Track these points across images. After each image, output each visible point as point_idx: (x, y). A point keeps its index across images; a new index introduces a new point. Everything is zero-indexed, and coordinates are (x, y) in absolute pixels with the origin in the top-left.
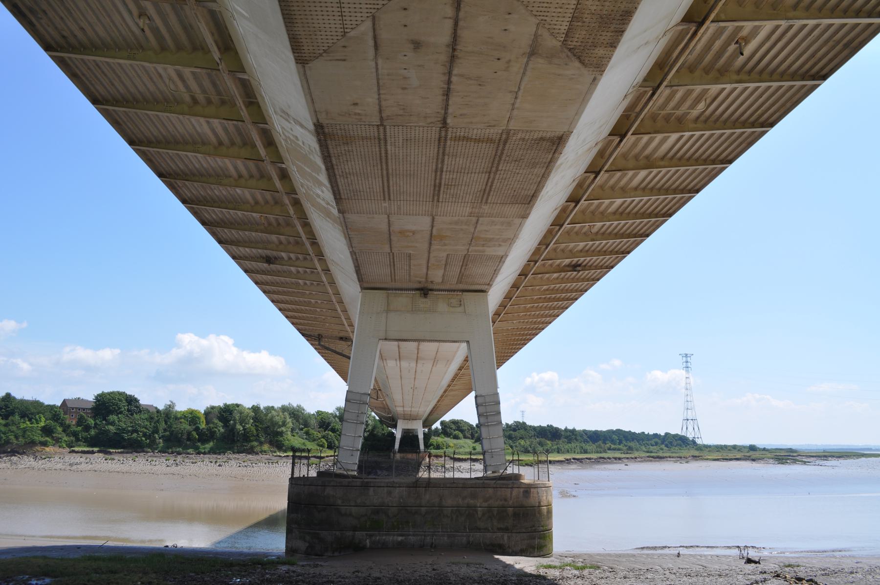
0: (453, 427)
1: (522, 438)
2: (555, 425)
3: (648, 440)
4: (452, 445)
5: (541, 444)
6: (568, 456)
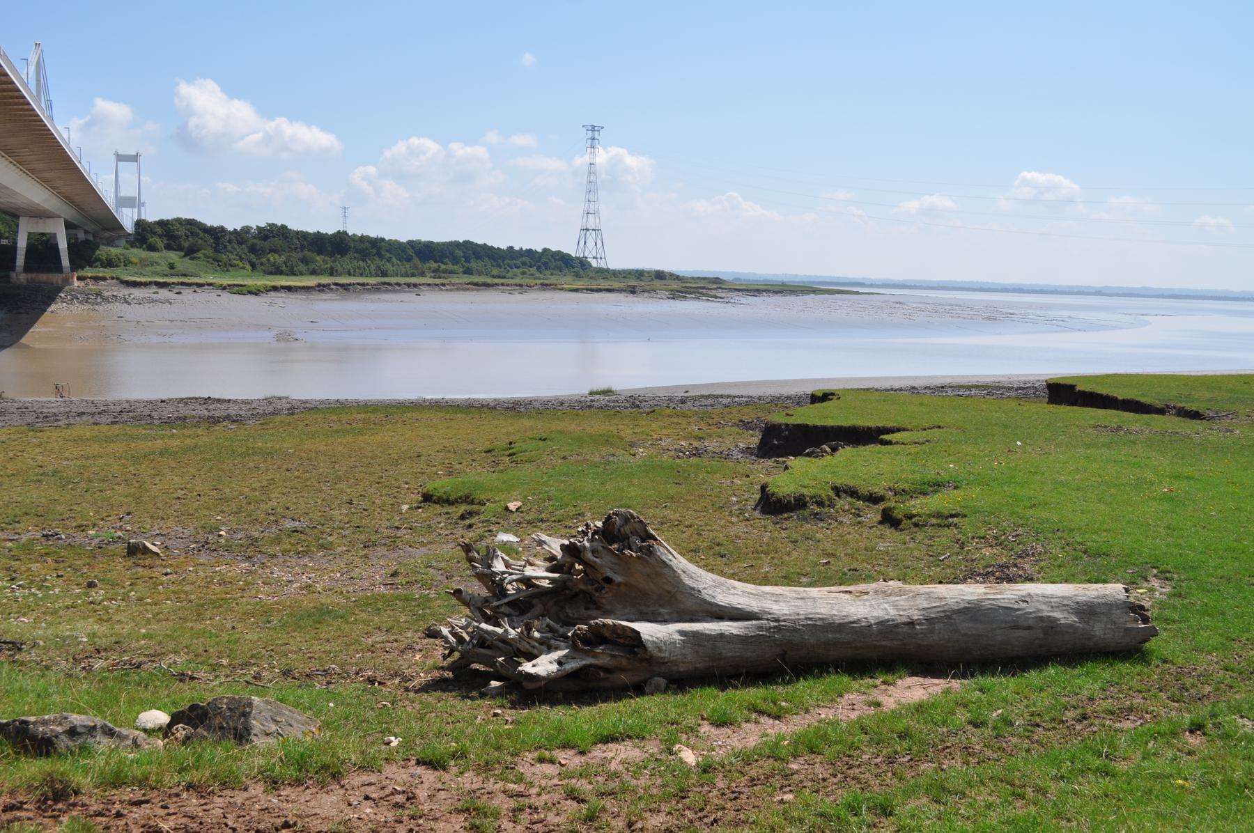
0: (159, 230)
1: (272, 251)
2: (489, 244)
3: (512, 258)
4: (135, 260)
5: (305, 261)
6: (325, 280)
